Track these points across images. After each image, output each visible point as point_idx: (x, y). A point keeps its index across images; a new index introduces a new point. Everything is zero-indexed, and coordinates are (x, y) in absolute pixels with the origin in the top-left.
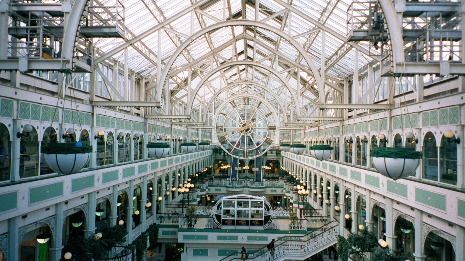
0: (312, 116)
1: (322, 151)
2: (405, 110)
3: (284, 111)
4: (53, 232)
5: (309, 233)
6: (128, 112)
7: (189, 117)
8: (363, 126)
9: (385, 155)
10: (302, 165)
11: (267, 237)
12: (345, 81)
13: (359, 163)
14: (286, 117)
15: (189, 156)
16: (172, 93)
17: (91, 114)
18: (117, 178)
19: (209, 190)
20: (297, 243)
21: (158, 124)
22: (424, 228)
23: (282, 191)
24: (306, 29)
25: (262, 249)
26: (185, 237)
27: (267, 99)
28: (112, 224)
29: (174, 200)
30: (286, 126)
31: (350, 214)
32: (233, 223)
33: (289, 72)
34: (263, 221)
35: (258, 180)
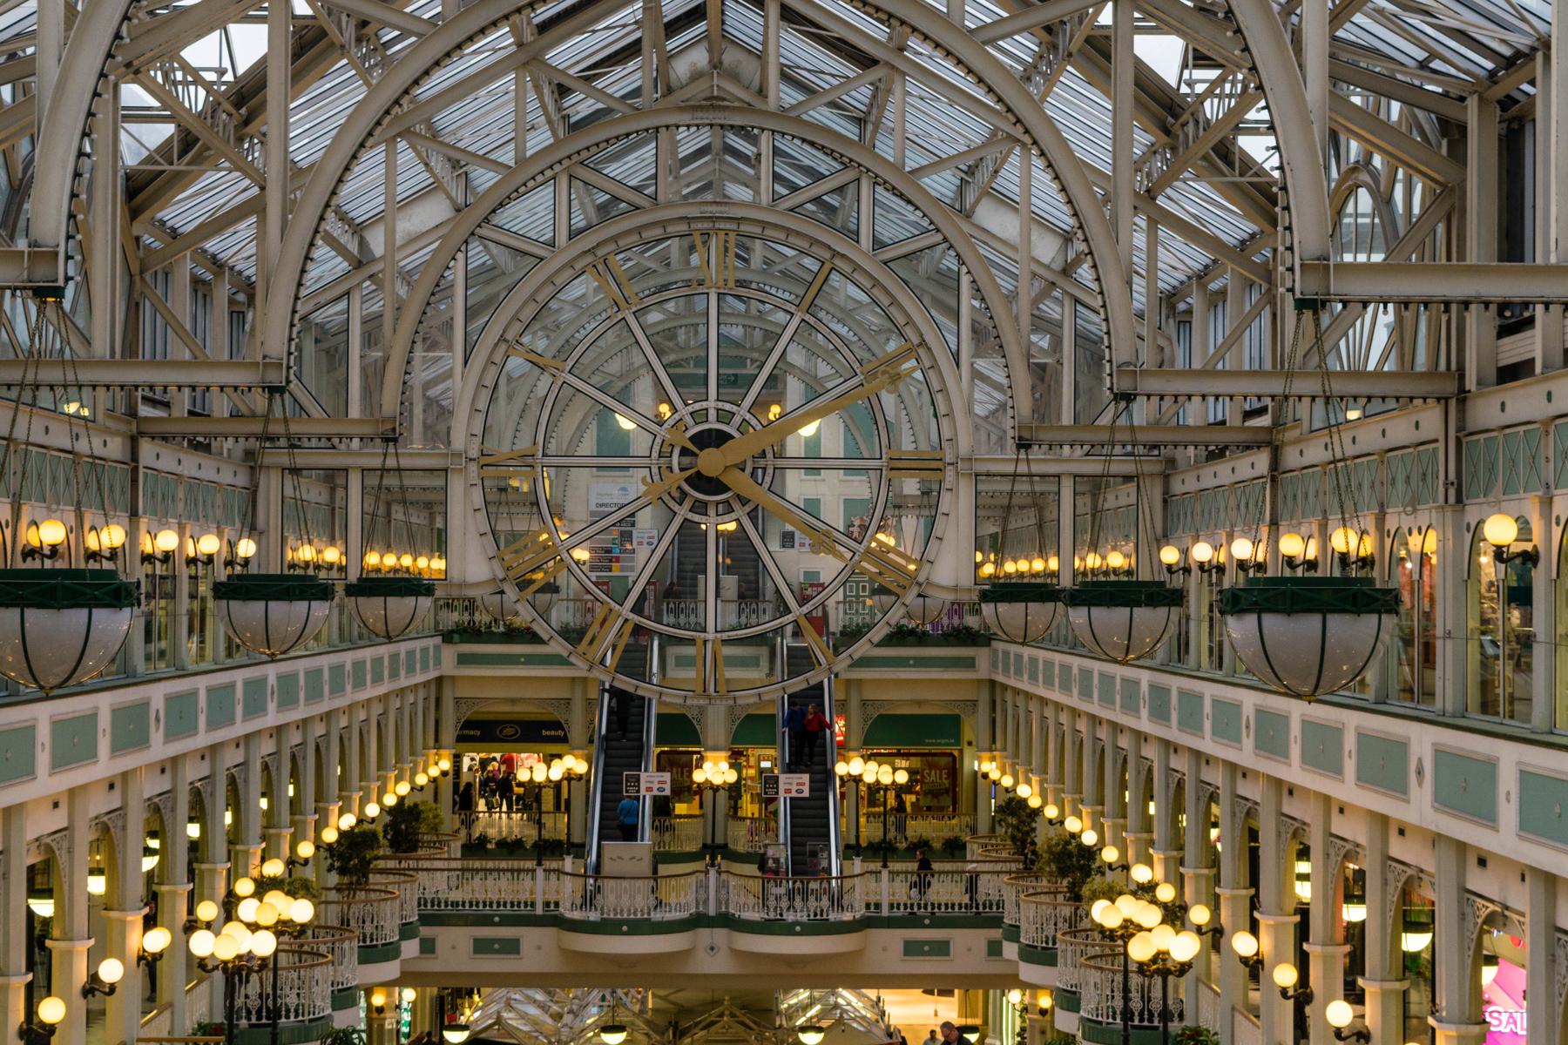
0: (1228, 363)
3: (1008, 337)
7: (275, 378)
12: (1472, 103)
14: (1023, 380)
15: (272, 680)
19: (428, 947)
23: (994, 949)
27: (878, 244)
28: (520, 752)
30: (1023, 445)
33: (1049, 29)
35: (806, 863)
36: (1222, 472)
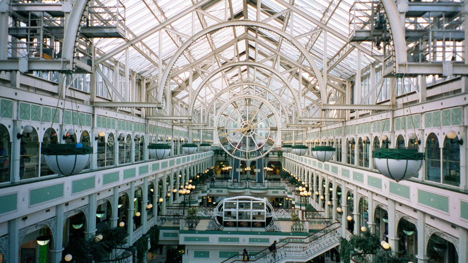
0: (314, 117)
1: (324, 152)
2: (407, 111)
4: (53, 234)
5: (311, 235)
6: (128, 113)
7: (190, 118)
8: (365, 127)
9: (387, 156)
10: (304, 167)
11: (268, 239)
12: (347, 82)
13: (361, 164)
14: (288, 118)
15: (191, 157)
16: (173, 93)
17: (91, 115)
18: (118, 179)
19: (211, 191)
20: (299, 245)
21: (159, 124)
22: (427, 229)
23: (284, 192)
24: (308, 29)
25: (264, 250)
26: (186, 239)
27: (269, 100)
29: (175, 202)
30: (288, 127)
31: (352, 215)
32: (235, 224)
33: (291, 72)
34: (264, 222)
36: (314, 130)
